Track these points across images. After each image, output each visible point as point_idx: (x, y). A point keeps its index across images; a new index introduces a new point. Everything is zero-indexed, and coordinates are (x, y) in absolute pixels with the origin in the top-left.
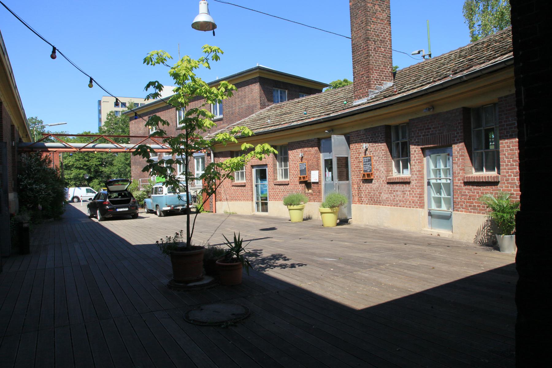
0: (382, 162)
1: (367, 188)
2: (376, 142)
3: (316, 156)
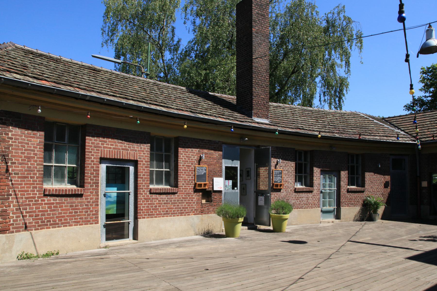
0: (291, 176)
1: (276, 196)
2: (286, 160)
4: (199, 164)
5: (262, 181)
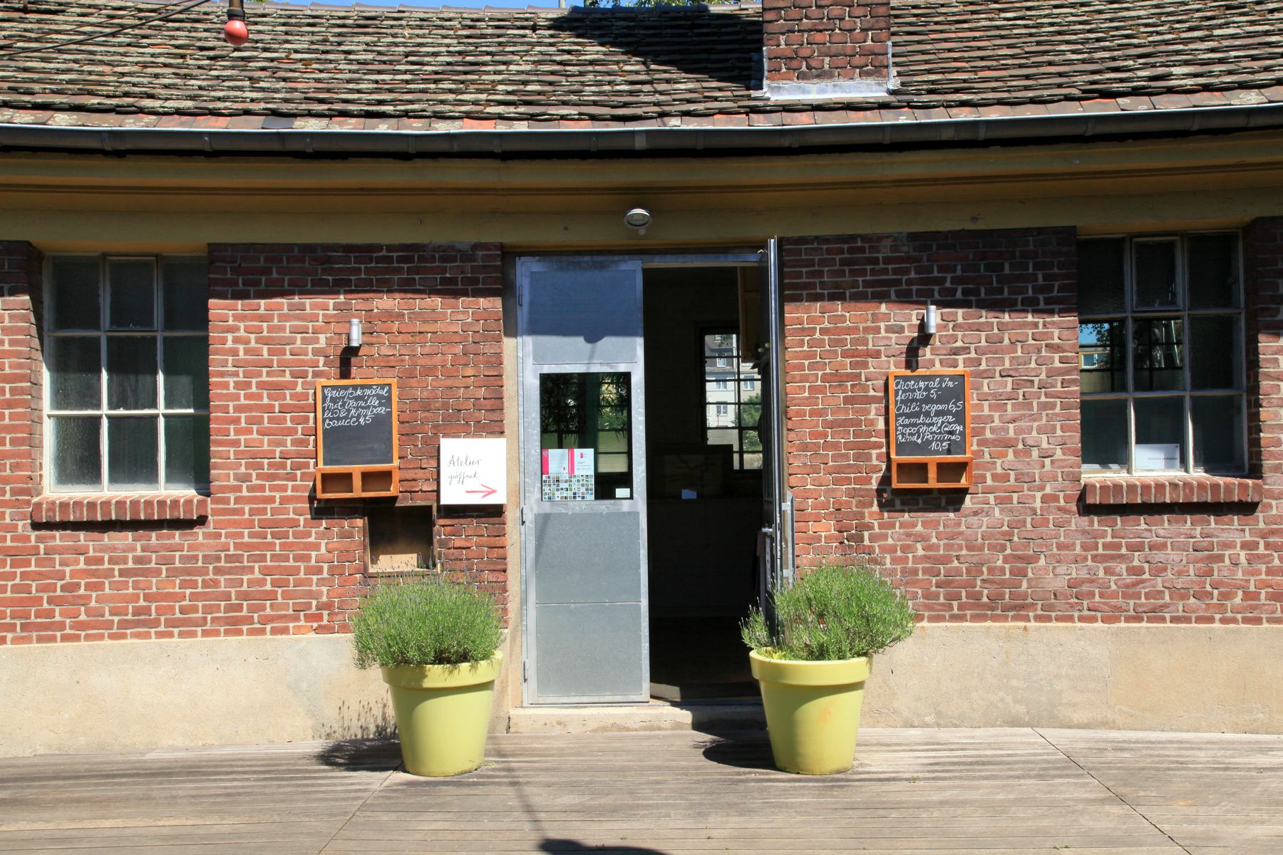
1: (923, 538)
3: (489, 349)
4: (345, 374)
5: (805, 447)
